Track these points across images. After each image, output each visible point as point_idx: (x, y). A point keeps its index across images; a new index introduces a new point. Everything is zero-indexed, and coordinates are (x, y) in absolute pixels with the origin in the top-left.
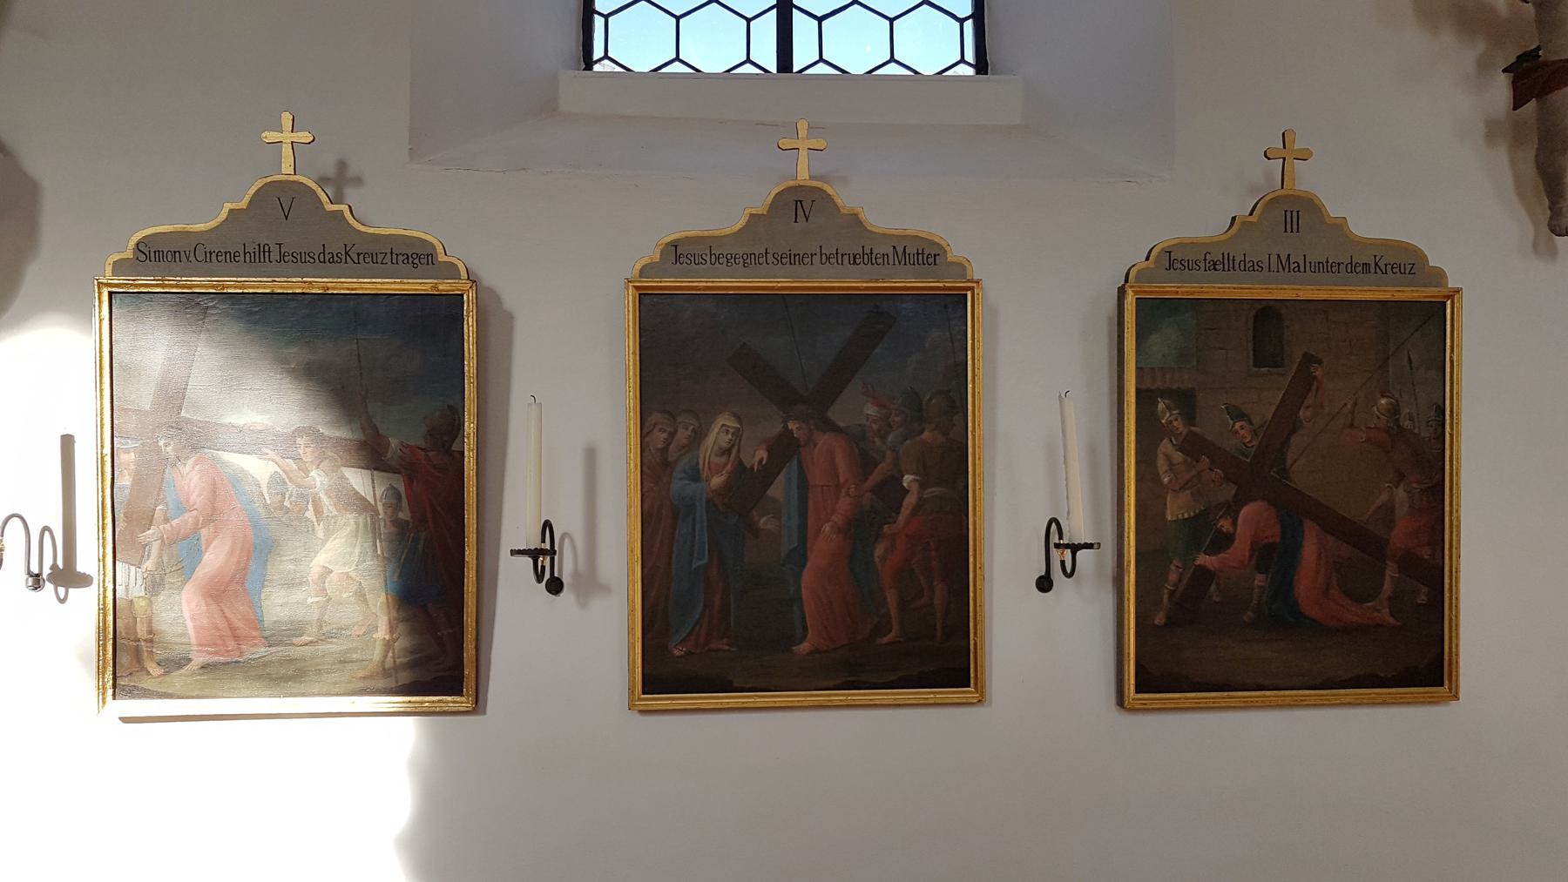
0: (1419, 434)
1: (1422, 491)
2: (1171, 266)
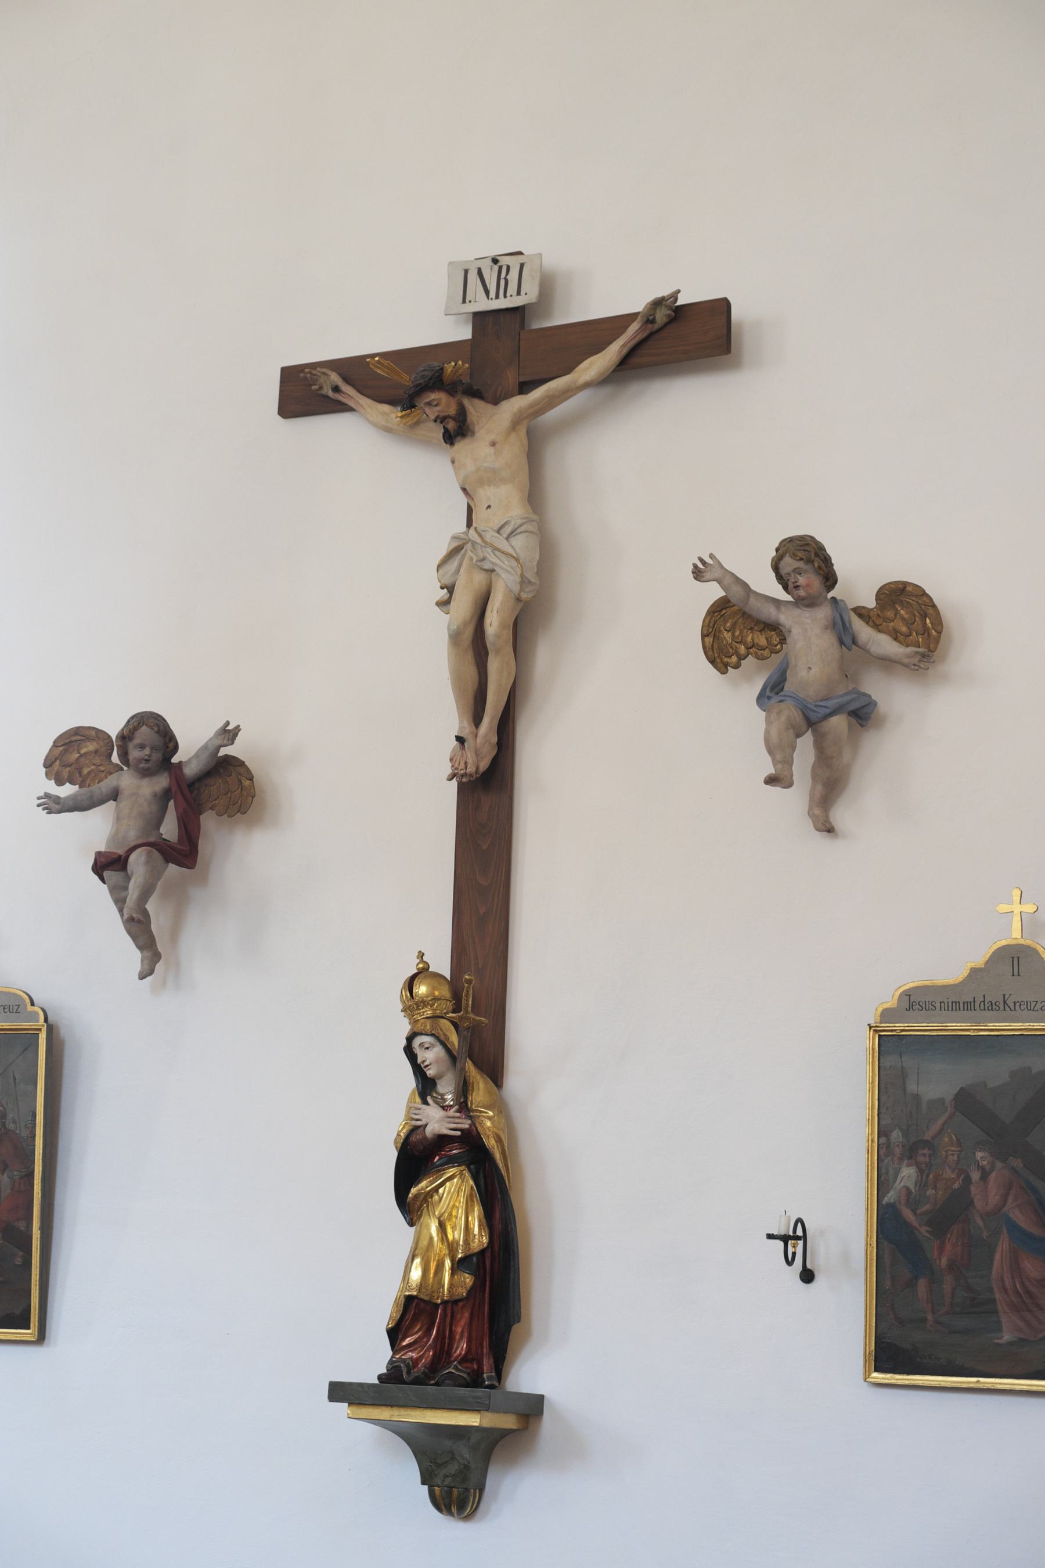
0: (20, 1134)
2: (911, 1007)
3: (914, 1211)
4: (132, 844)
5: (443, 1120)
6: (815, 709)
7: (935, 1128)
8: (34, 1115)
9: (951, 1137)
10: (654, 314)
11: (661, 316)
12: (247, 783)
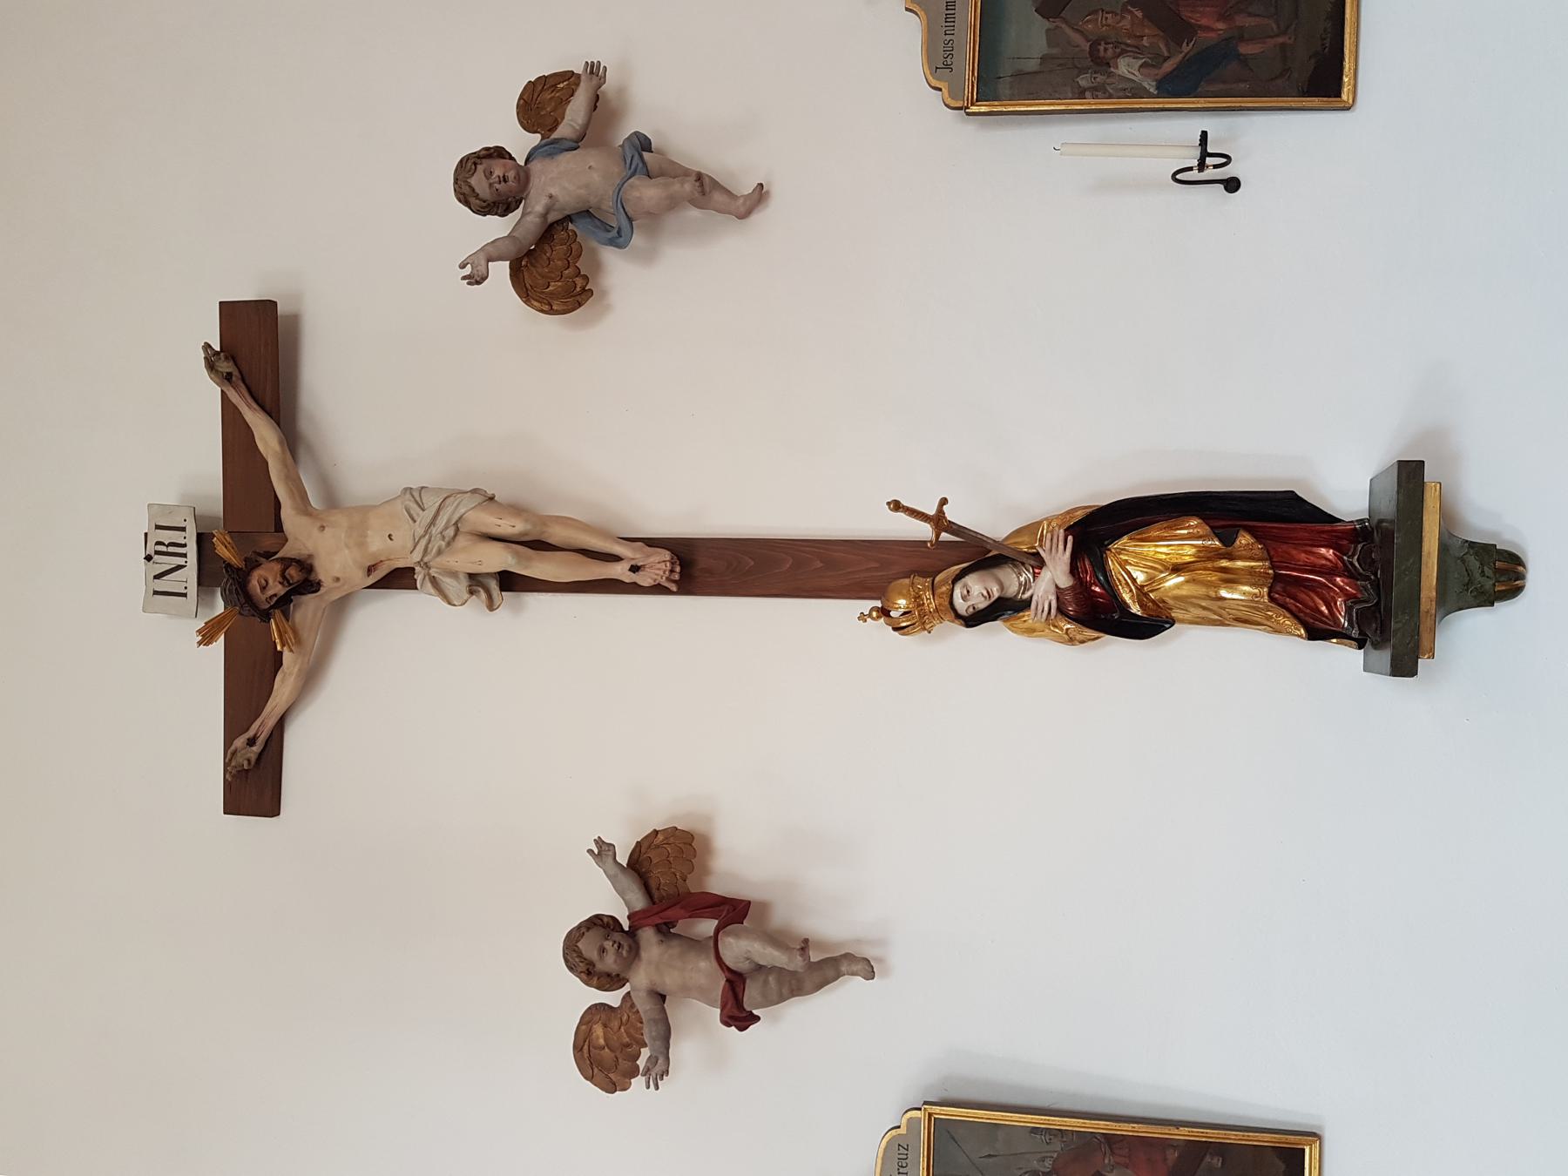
1: (1112, 1153)
2: (947, 66)
3: (1166, 59)
4: (715, 964)
5: (1054, 559)
6: (632, 170)
7: (1077, 38)
8: (1034, 1130)
9: (1088, 21)
10: (222, 373)
11: (225, 366)
12: (661, 837)
